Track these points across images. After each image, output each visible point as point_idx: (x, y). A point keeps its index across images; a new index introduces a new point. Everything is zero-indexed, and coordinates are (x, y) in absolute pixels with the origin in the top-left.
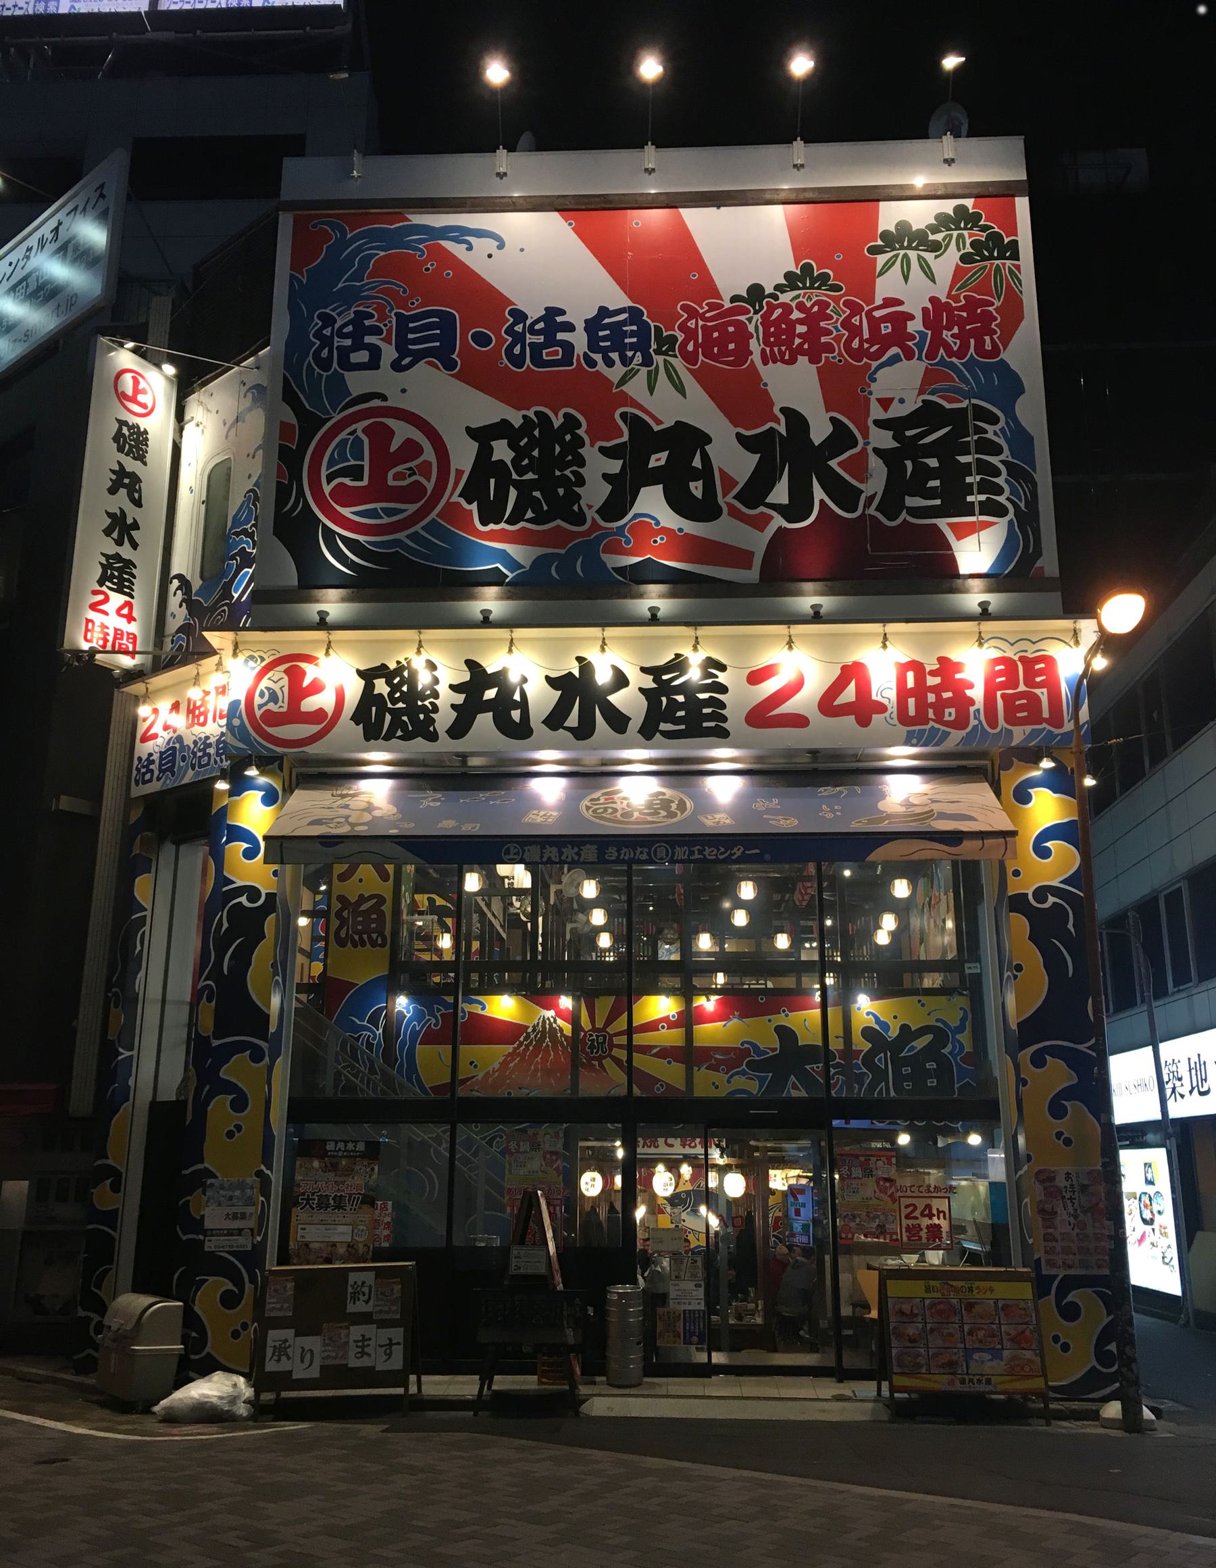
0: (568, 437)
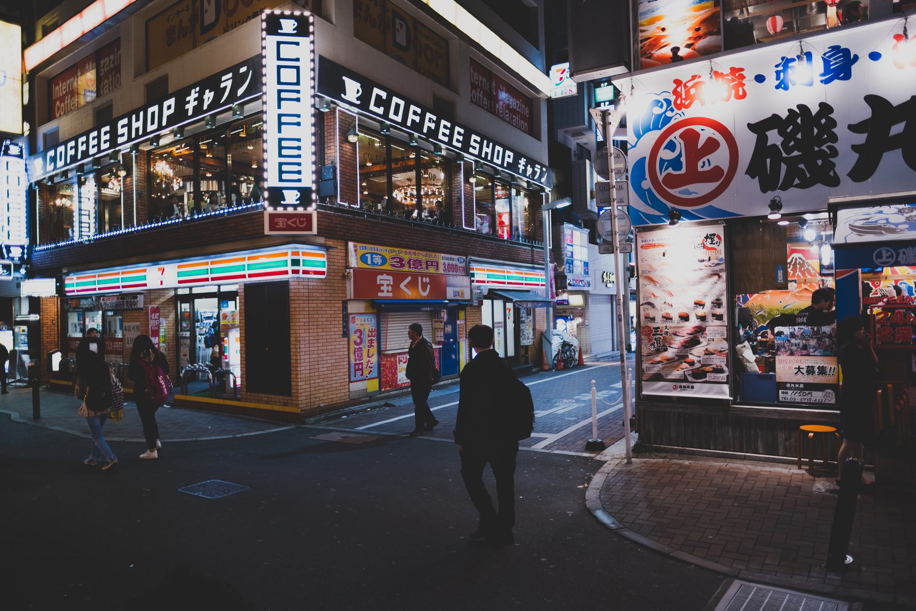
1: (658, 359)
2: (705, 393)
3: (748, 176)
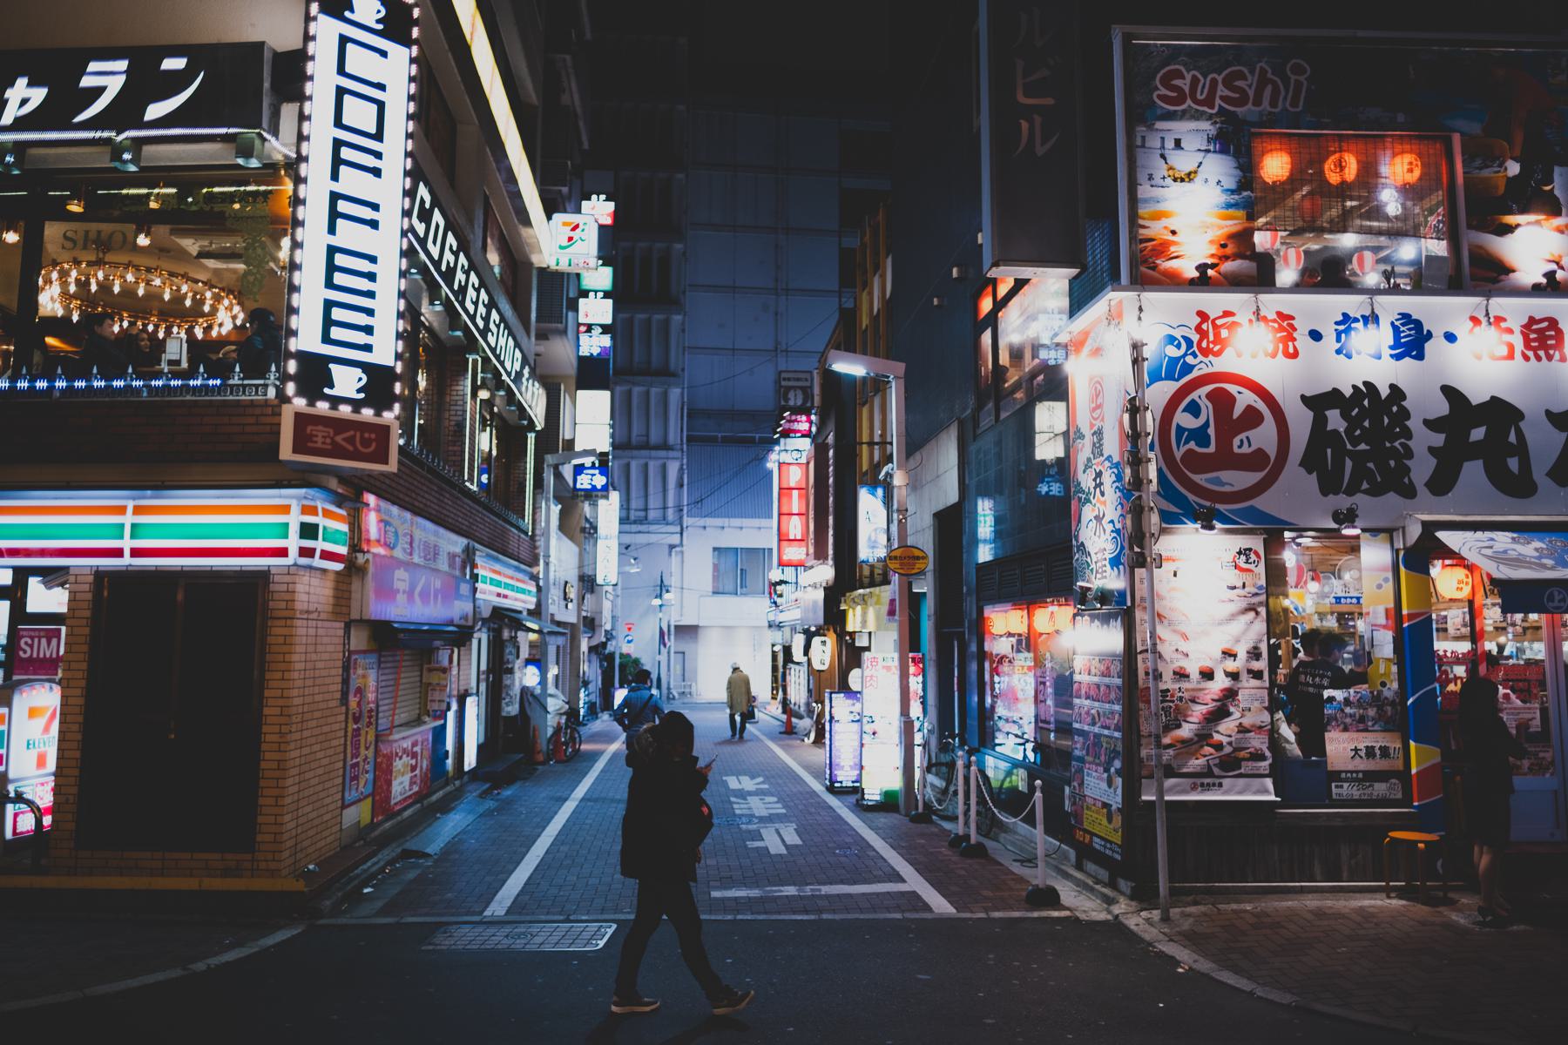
0: (1395, 409)
2: (1240, 793)
3: (1302, 470)
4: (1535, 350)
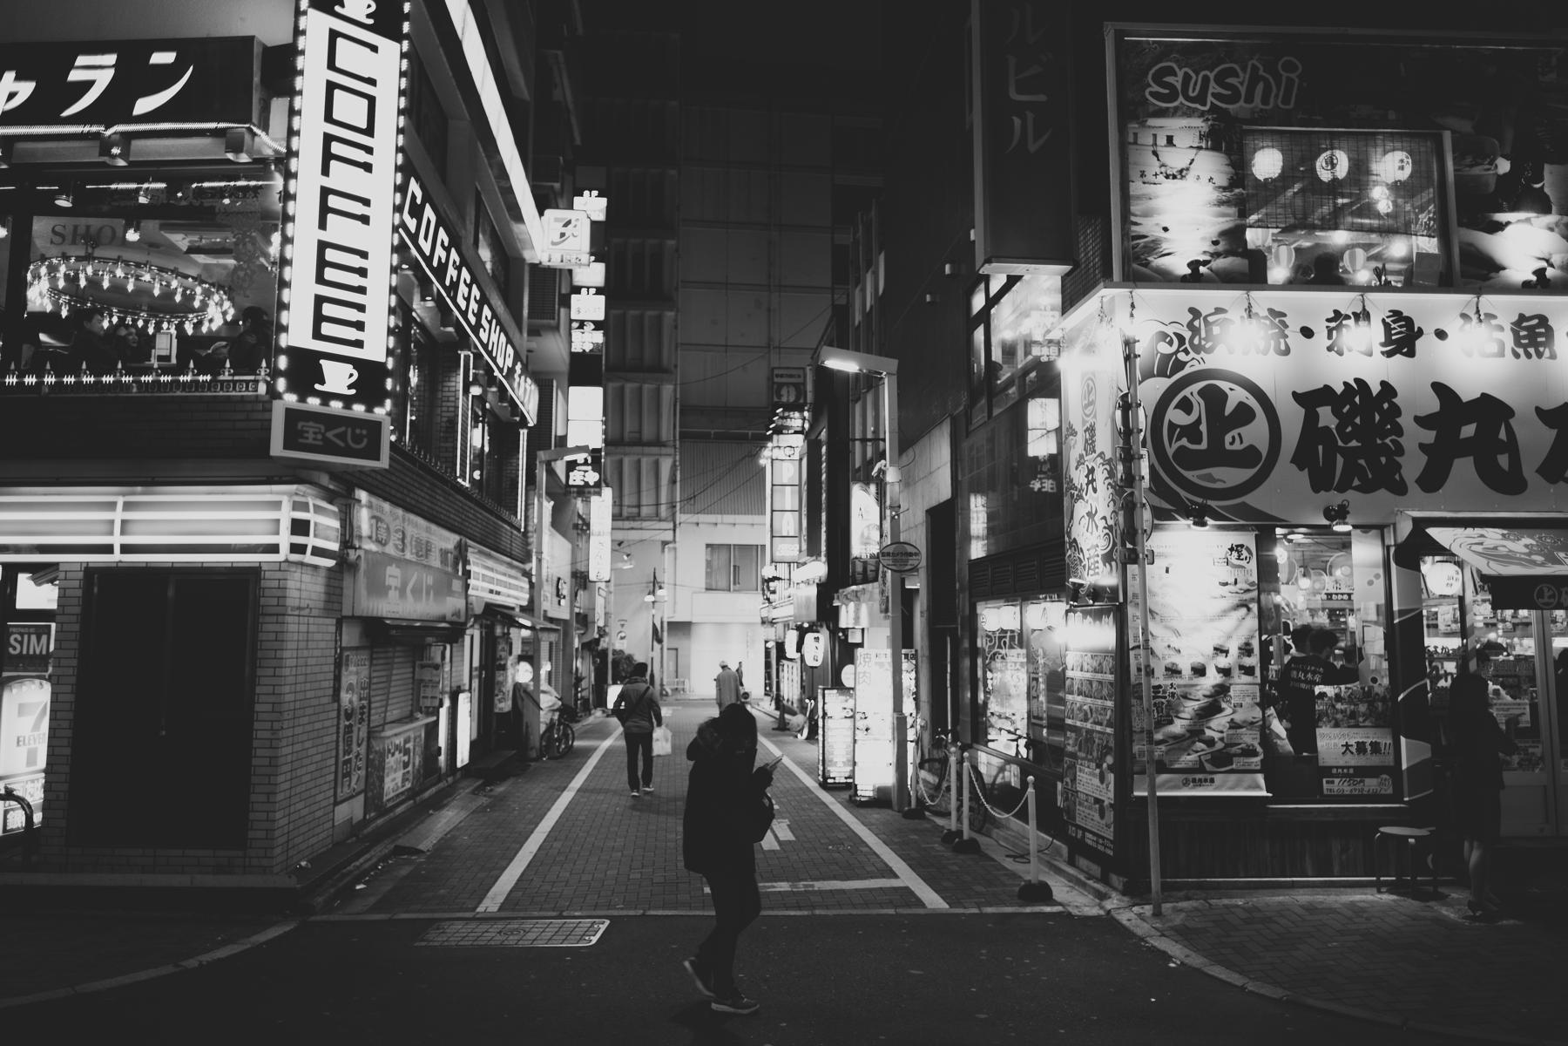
0: (1386, 406)
1: (1158, 736)
2: (1232, 788)
4: (1525, 347)
